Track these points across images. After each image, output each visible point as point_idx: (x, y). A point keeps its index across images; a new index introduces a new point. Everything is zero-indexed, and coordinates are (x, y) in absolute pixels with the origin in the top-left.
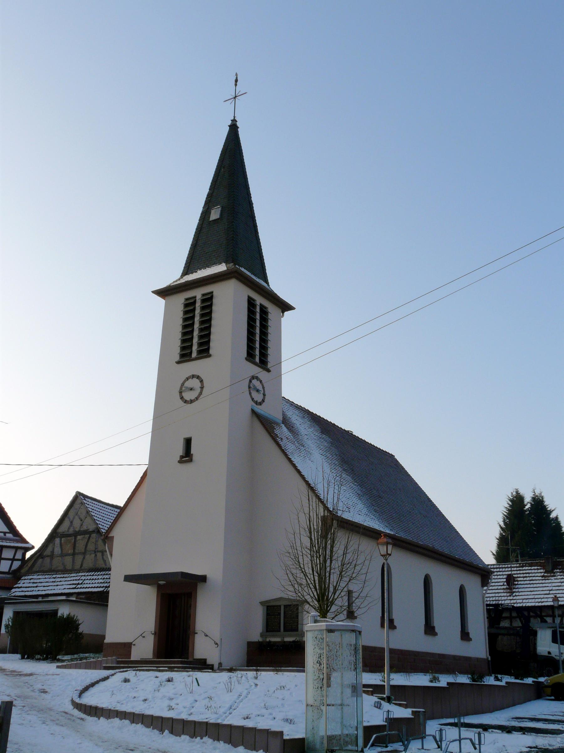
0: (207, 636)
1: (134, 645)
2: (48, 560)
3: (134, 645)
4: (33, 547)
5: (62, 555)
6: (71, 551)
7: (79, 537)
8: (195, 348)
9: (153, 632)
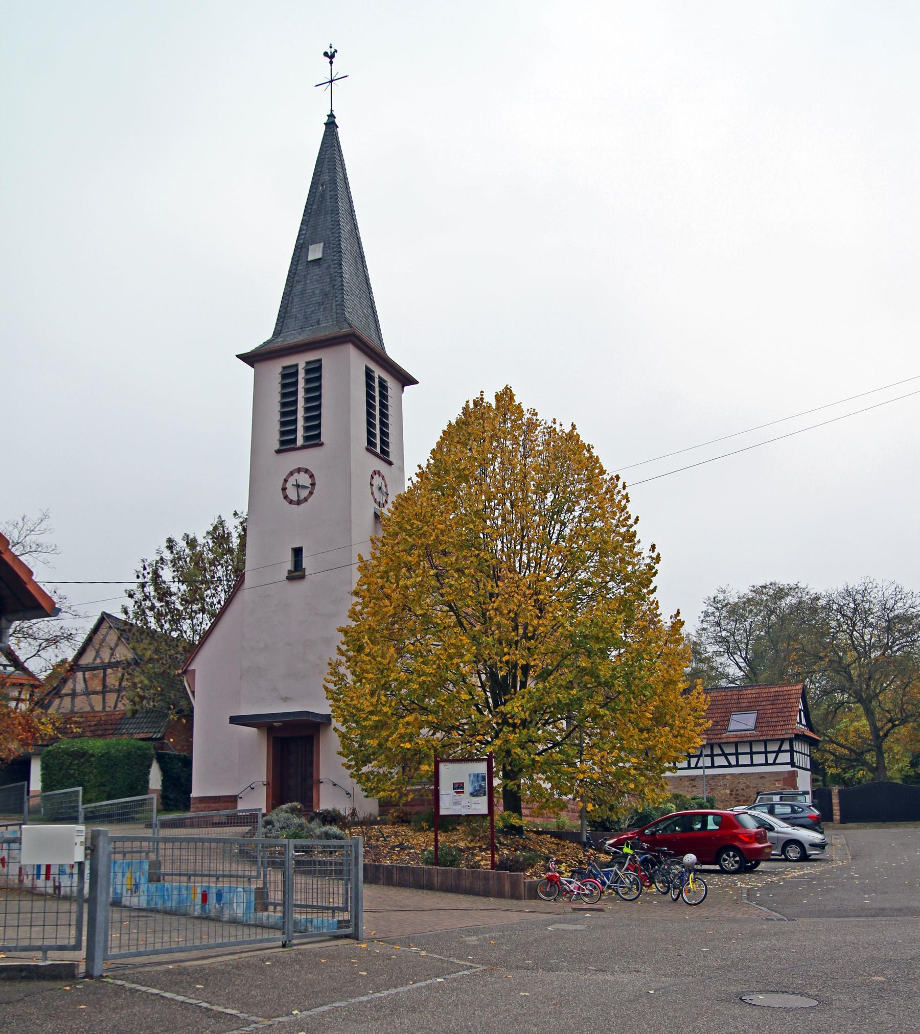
0: (335, 785)
1: (241, 798)
2: (67, 701)
3: (241, 798)
5: (87, 693)
6: (99, 688)
9: (265, 783)
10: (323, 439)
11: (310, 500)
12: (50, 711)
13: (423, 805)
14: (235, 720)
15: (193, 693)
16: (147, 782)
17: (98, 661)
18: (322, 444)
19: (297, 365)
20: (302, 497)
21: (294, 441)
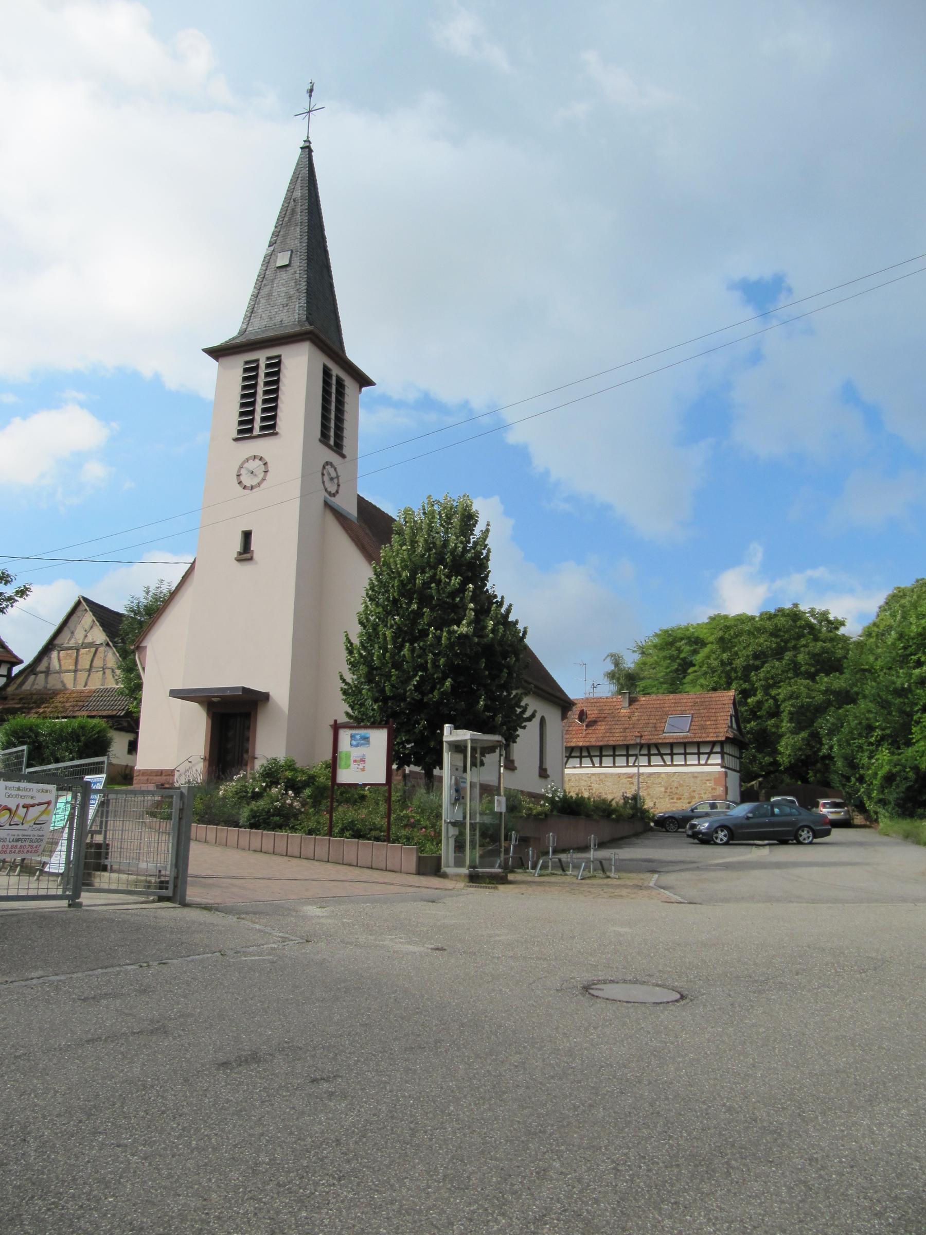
2: (42, 677)
4: (21, 662)
7: (82, 651)
8: (257, 424)
14: (175, 694)
18: (276, 434)
19: (257, 361)
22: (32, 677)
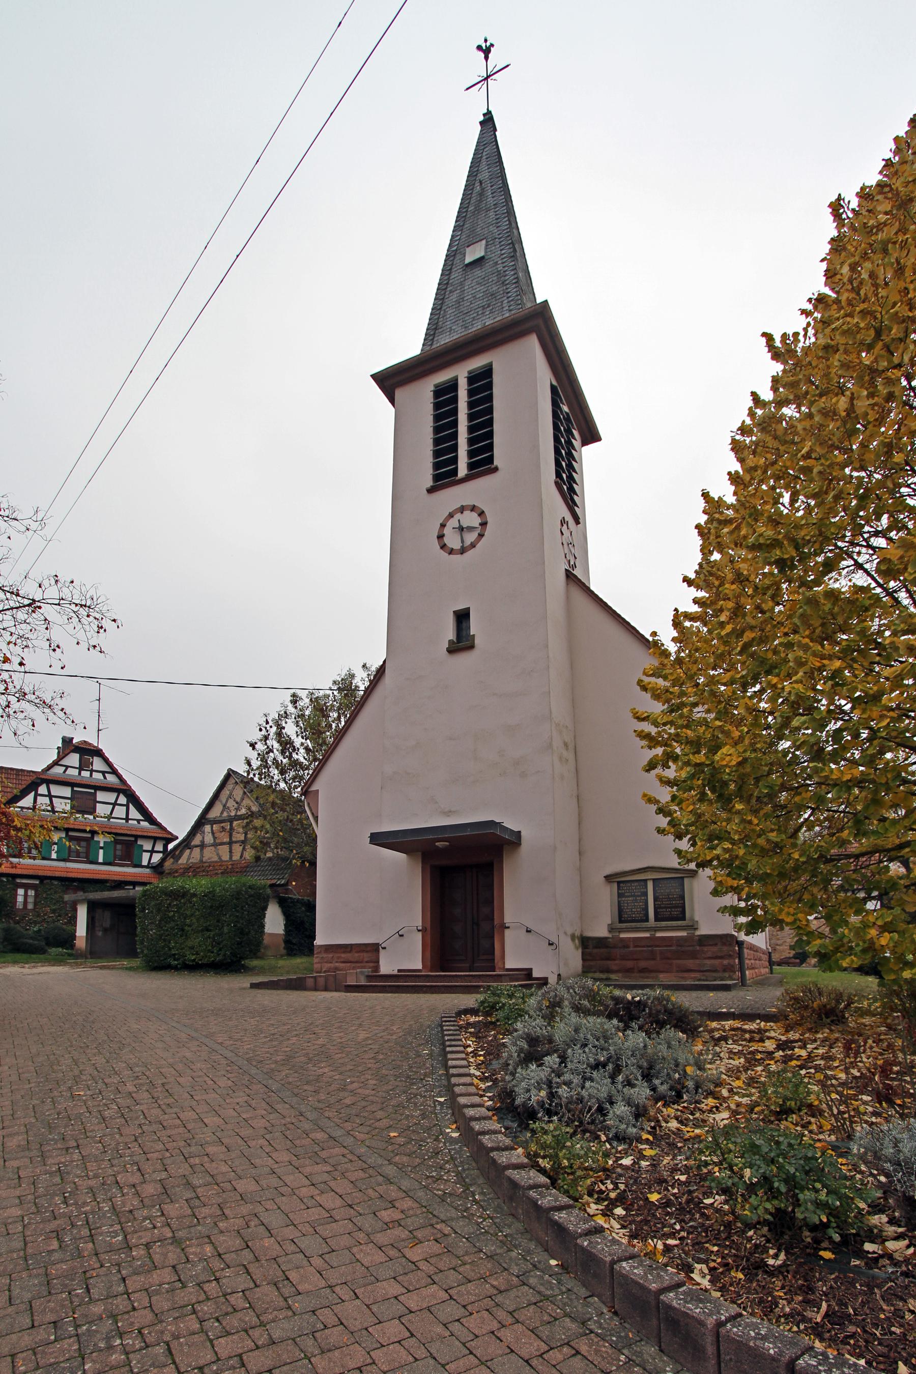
0: (528, 931)
1: (384, 948)
2: (197, 851)
3: (384, 948)
4: (177, 838)
5: (215, 845)
7: (235, 823)
9: (420, 928)
10: (496, 462)
11: (478, 546)
12: (180, 862)
13: (654, 959)
14: (377, 839)
15: (316, 818)
16: (263, 926)
17: (225, 814)
18: (496, 469)
20: (468, 542)
21: (455, 472)
22: (188, 851)
